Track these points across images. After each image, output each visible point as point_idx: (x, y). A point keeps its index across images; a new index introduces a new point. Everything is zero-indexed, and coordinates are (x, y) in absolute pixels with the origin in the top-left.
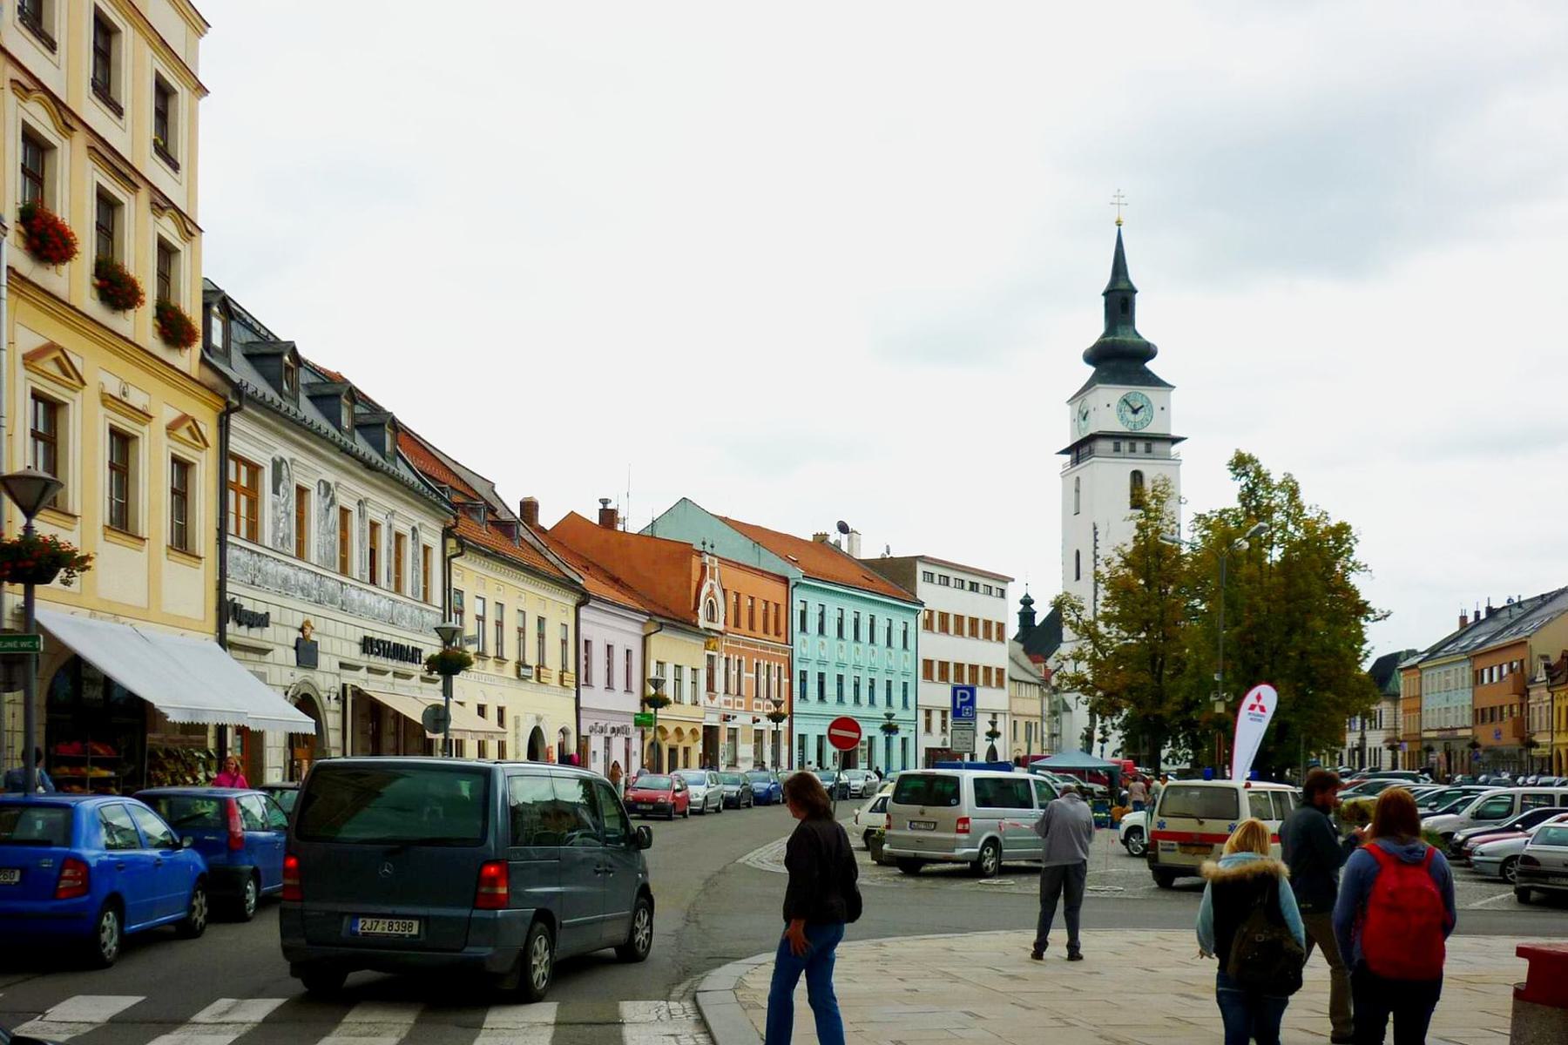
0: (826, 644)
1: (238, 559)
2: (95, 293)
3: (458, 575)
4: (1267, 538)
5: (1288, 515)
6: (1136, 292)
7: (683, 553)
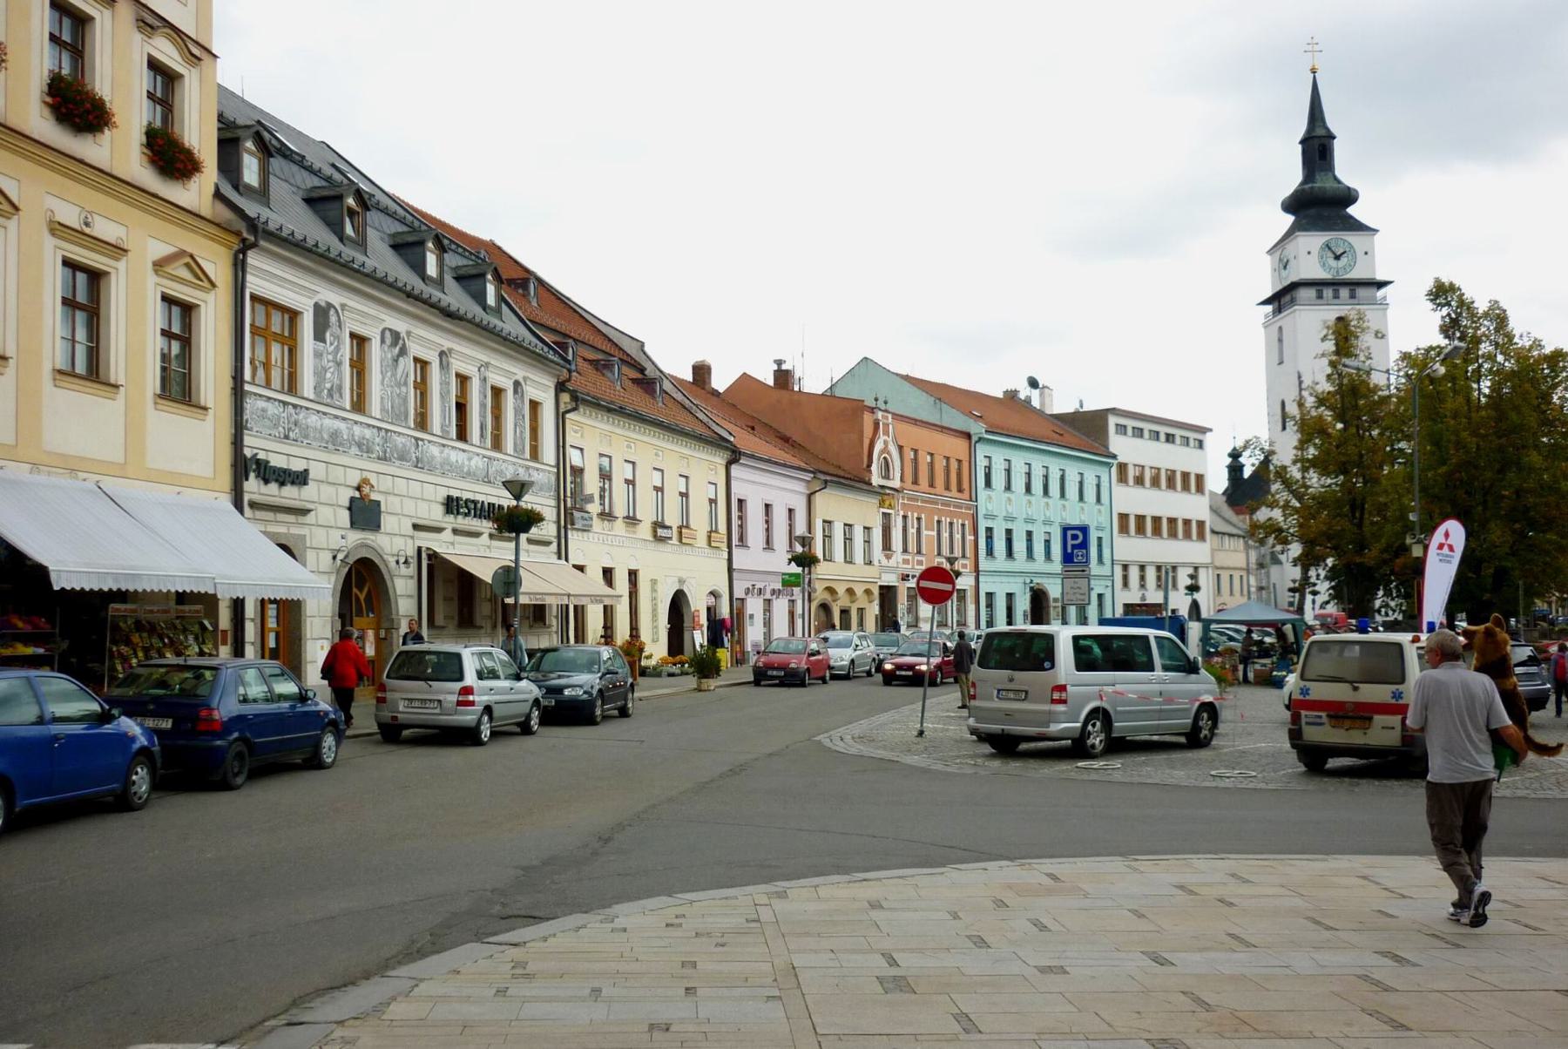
0: (1033, 502)
1: (264, 410)
2: (47, 112)
3: (576, 432)
4: (1473, 371)
5: (1497, 344)
6: (1334, 138)
7: (857, 409)
